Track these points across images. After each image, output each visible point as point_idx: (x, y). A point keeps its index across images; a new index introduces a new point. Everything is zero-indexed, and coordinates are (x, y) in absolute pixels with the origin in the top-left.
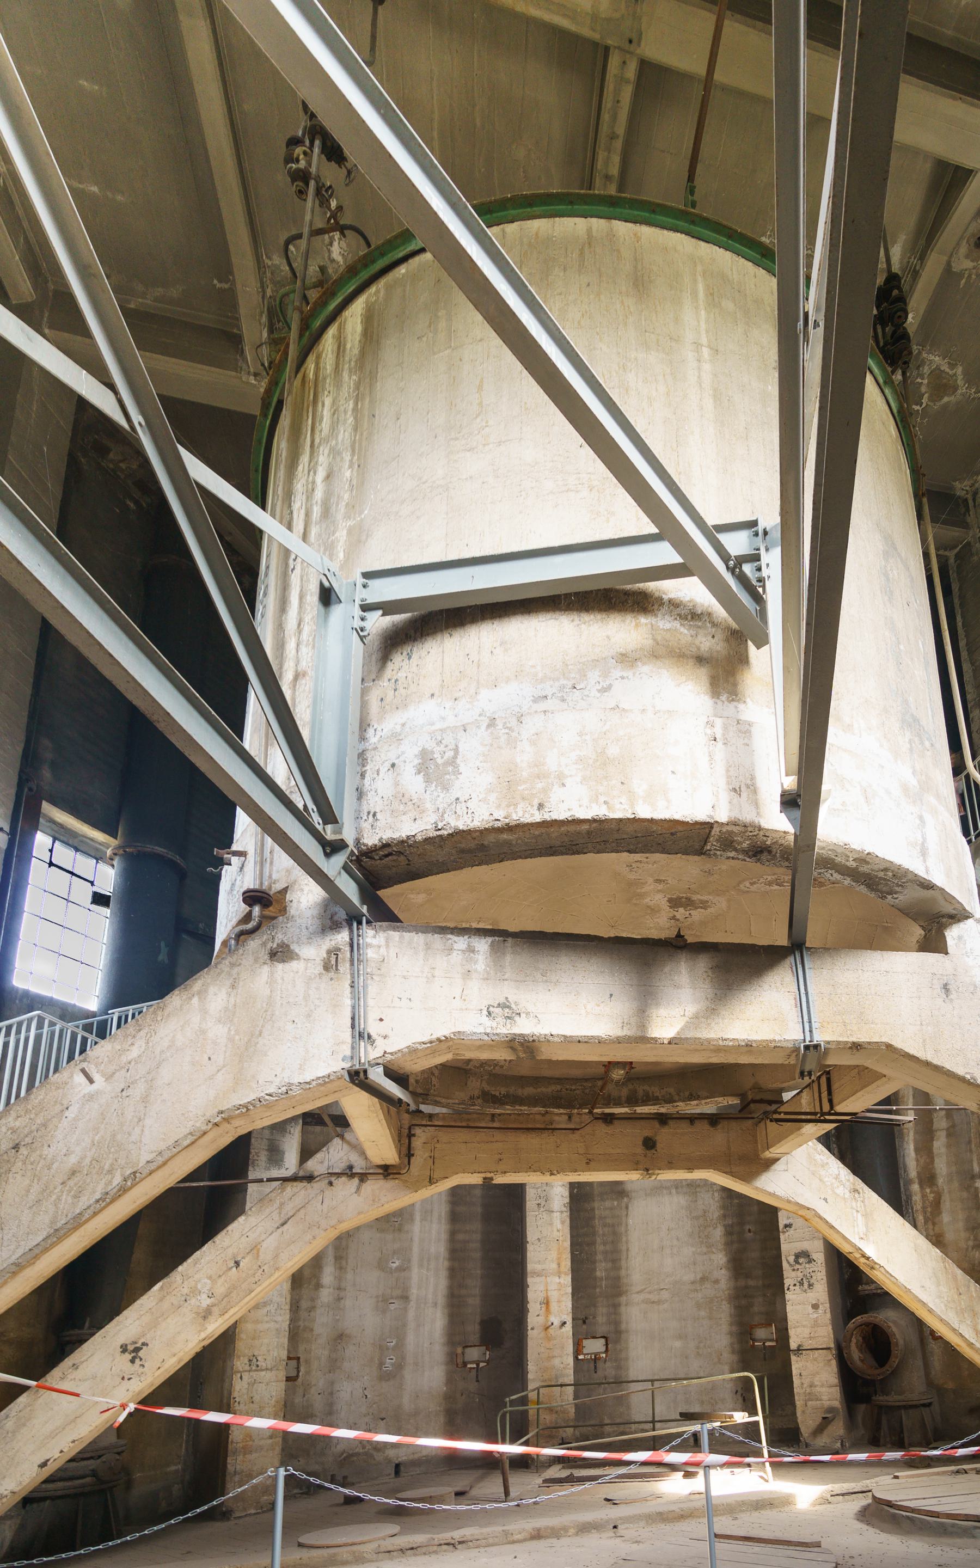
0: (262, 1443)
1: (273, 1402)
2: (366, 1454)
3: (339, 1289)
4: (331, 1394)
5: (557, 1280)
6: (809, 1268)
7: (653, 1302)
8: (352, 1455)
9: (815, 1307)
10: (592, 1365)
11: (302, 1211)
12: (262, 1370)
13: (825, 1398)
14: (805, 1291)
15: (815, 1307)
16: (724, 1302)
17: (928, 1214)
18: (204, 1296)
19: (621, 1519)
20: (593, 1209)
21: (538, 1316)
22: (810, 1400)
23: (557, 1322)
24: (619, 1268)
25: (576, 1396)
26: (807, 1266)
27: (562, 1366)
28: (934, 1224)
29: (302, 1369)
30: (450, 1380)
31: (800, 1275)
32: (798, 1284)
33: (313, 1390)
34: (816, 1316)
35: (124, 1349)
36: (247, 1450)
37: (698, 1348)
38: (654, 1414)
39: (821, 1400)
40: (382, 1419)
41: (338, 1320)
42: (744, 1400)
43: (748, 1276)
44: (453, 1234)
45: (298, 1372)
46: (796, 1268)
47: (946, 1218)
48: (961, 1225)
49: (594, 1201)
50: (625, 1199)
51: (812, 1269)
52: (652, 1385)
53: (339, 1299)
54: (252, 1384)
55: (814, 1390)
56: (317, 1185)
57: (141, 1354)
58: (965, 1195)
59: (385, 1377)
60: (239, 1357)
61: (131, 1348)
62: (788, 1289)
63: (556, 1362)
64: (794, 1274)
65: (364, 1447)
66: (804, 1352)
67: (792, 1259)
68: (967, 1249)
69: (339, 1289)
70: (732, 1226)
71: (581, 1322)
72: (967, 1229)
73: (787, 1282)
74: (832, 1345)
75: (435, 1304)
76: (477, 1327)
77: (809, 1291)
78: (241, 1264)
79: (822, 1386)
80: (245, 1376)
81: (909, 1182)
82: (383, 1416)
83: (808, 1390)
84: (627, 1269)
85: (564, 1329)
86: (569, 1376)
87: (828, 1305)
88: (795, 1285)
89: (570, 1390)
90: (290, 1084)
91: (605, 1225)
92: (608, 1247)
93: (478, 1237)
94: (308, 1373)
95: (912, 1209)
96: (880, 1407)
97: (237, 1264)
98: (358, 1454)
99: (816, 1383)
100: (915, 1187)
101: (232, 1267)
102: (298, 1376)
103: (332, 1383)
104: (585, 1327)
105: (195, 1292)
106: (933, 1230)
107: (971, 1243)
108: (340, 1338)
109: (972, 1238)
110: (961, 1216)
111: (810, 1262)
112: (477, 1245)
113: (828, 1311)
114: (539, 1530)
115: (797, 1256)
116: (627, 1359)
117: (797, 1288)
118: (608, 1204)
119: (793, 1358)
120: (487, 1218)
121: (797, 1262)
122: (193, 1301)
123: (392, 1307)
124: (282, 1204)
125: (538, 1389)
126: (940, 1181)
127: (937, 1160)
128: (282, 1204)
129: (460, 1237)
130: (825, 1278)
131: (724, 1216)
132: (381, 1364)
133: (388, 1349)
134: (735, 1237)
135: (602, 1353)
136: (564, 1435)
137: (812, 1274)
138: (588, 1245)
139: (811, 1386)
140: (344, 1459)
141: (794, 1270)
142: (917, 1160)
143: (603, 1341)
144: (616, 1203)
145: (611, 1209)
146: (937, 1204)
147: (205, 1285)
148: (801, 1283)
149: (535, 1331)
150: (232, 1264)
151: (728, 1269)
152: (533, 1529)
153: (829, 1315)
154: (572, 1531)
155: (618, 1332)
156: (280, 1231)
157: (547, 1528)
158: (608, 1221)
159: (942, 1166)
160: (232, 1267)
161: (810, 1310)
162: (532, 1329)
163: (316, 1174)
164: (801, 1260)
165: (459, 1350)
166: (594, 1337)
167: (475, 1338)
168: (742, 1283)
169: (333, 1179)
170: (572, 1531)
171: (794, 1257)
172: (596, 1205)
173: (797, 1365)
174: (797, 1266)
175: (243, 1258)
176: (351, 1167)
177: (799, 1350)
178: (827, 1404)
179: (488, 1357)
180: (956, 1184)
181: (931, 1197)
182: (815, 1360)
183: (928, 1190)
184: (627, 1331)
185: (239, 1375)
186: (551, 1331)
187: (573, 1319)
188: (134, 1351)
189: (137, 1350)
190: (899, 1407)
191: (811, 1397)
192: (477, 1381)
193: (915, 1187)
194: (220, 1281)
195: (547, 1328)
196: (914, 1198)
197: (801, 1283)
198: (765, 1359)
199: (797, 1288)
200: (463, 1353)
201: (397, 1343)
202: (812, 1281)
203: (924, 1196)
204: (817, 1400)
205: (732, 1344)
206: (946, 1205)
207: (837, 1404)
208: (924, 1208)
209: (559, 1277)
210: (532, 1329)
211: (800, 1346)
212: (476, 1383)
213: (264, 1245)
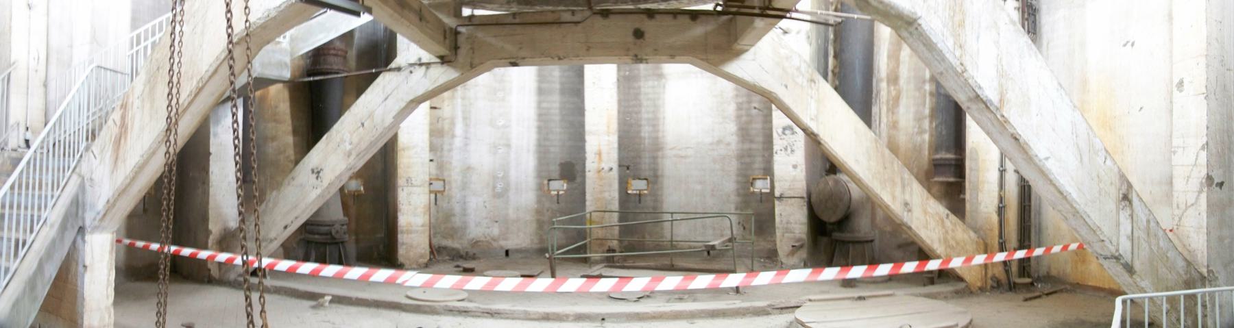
0: (417, 228)
1: (422, 206)
2: (487, 242)
3: (466, 138)
4: (465, 203)
5: (607, 138)
6: (793, 138)
7: (682, 157)
8: (480, 241)
9: (795, 167)
10: (637, 198)
11: (396, 91)
12: (415, 186)
13: (797, 231)
14: (788, 155)
15: (795, 167)
16: (734, 160)
17: (890, 106)
18: (347, 144)
19: (607, 314)
20: (639, 87)
21: (593, 162)
22: (787, 232)
23: (606, 168)
24: (658, 131)
25: (621, 220)
26: (791, 136)
27: (610, 198)
28: (893, 113)
29: (447, 187)
30: (539, 201)
31: (785, 143)
32: (783, 149)
33: (453, 200)
34: (794, 173)
35: (313, 171)
36: (409, 232)
37: (713, 191)
38: (672, 236)
39: (794, 233)
40: (497, 222)
41: (466, 158)
42: (744, 228)
43: (751, 141)
44: (539, 103)
45: (445, 188)
46: (782, 137)
47: (902, 110)
48: (911, 116)
49: (640, 81)
50: (664, 80)
51: (793, 140)
52: (672, 217)
53: (466, 145)
54: (409, 194)
55: (789, 225)
56: (404, 74)
57: (321, 174)
58: (917, 94)
59: (497, 196)
60: (400, 178)
61: (316, 171)
62: (776, 153)
63: (606, 195)
64: (780, 142)
65: (486, 237)
66: (784, 199)
67: (780, 131)
68: (913, 134)
69: (466, 138)
70: (741, 103)
71: (626, 168)
72: (915, 120)
73: (776, 148)
74: (805, 195)
75: (529, 151)
76: (558, 168)
77: (791, 155)
78: (365, 125)
79: (796, 223)
80: (405, 189)
81: (879, 81)
82: (497, 220)
83: (785, 226)
84: (663, 132)
85: (611, 173)
86: (615, 206)
87: (804, 166)
88: (781, 150)
89: (616, 215)
90: (269, 10)
91: (648, 99)
92: (651, 116)
93: (557, 105)
94: (450, 189)
95: (880, 101)
96: (837, 241)
97: (363, 124)
98: (482, 241)
99: (792, 221)
100: (884, 85)
101: (360, 127)
102: (444, 191)
103: (465, 196)
104: (628, 172)
105: (343, 141)
106: (892, 118)
107: (916, 130)
108: (468, 169)
109: (917, 126)
110: (912, 110)
111: (793, 134)
112: (557, 111)
113: (804, 170)
114: (548, 314)
115: (784, 129)
116: (662, 195)
117: (783, 152)
118: (650, 83)
119: (777, 203)
120: (563, 92)
121: (784, 133)
122: (342, 146)
123: (500, 151)
124: (384, 87)
125: (590, 213)
126: (902, 82)
127: (901, 66)
128: (384, 87)
129: (544, 105)
130: (803, 146)
131: (737, 96)
132: (494, 187)
133: (498, 178)
134: (743, 112)
135: (645, 190)
136: (611, 245)
137: (795, 143)
138: (636, 113)
139: (787, 223)
140: (475, 243)
141: (781, 139)
142: (888, 65)
143: (645, 182)
144: (656, 83)
145: (653, 87)
146: (897, 99)
147: (347, 137)
148: (786, 149)
149: (590, 173)
150: (360, 124)
151: (737, 135)
152: (544, 313)
153: (804, 173)
154: (571, 318)
155: (656, 176)
156: (384, 103)
157: (554, 314)
158: (650, 96)
159: (904, 72)
160: (360, 127)
161: (791, 168)
162: (589, 171)
163: (402, 66)
164: (787, 132)
165: (546, 182)
166: (640, 179)
167: (556, 174)
168: (747, 146)
169: (412, 69)
170: (571, 318)
171: (781, 130)
172: (642, 84)
173: (779, 208)
174: (784, 136)
175: (366, 121)
176: (420, 59)
177: (781, 198)
178: (798, 236)
179: (565, 188)
180: (912, 86)
181: (894, 93)
182: (792, 205)
183: (892, 88)
184: (662, 176)
185: (401, 189)
186: (602, 174)
187: (620, 166)
188: (317, 173)
189: (318, 172)
190: (849, 242)
191: (787, 230)
192: (558, 203)
193: (884, 85)
194: (355, 135)
195: (599, 172)
196: (882, 93)
197: (786, 149)
198: (761, 202)
199: (783, 152)
200: (548, 184)
201: (504, 175)
202: (794, 148)
203: (889, 92)
204: (791, 232)
205: (738, 190)
206: (903, 101)
207: (804, 236)
208: (888, 101)
209: (608, 136)
210: (589, 171)
211: (782, 194)
212: (557, 205)
213: (377, 112)
